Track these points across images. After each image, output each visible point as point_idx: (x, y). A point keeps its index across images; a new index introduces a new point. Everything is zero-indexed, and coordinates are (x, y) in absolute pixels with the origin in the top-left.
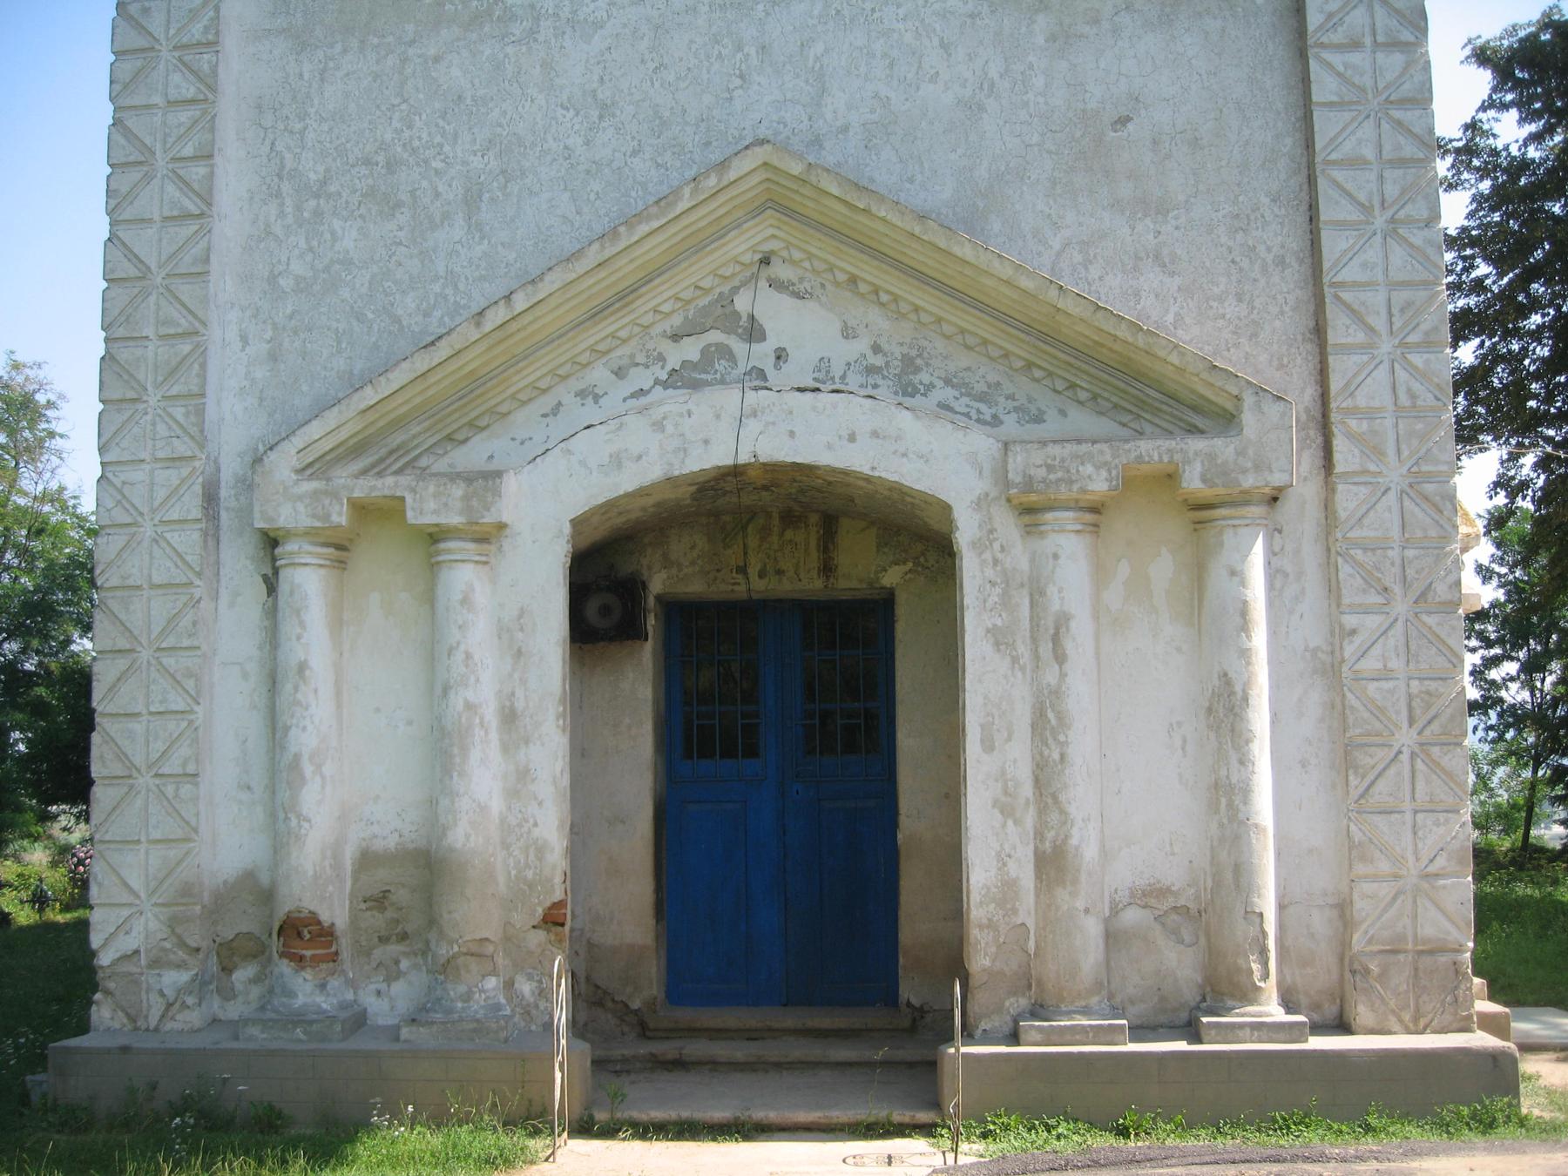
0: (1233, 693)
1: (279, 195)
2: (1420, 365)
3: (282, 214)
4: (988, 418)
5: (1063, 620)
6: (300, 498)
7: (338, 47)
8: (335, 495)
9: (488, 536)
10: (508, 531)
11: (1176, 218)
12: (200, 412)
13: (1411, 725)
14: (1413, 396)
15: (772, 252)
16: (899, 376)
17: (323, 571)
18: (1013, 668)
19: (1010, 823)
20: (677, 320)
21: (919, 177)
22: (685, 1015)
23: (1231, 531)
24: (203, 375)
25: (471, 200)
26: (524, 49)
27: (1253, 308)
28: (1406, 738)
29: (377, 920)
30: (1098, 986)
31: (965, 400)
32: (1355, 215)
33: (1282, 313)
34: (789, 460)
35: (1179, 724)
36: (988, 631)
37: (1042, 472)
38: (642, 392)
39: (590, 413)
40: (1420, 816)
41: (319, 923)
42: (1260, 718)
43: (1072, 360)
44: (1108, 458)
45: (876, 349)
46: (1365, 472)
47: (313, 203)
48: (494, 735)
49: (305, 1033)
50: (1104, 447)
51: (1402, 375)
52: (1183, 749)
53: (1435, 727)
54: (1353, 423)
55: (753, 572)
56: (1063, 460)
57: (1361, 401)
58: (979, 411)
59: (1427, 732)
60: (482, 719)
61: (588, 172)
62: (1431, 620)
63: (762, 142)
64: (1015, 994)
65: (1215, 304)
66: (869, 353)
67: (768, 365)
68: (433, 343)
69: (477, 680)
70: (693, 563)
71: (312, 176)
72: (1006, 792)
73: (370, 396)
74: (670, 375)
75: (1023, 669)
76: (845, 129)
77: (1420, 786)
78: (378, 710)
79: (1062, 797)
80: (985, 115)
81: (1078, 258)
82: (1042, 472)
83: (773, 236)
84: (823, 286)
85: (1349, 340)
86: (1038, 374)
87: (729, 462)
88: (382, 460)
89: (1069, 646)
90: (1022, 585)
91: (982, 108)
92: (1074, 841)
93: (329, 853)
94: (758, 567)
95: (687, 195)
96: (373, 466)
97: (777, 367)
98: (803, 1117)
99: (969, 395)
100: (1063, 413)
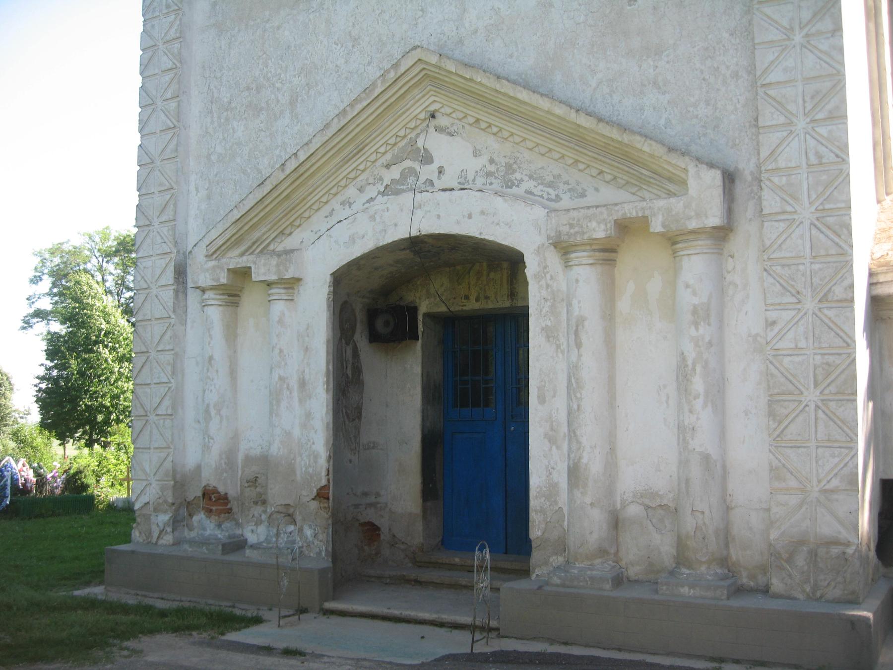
0: (686, 366)
1: (211, 112)
2: (825, 135)
3: (212, 122)
4: (553, 197)
5: (581, 321)
7: (236, 29)
9: (292, 284)
10: (302, 282)
11: (668, 56)
12: (174, 228)
13: (815, 388)
14: (819, 156)
15: (436, 111)
16: (504, 176)
17: (221, 308)
18: (557, 352)
19: (554, 447)
20: (389, 156)
21: (516, 54)
22: (444, 557)
23: (686, 258)
25: (293, 103)
26: (318, 14)
27: (716, 109)
28: (812, 396)
29: (251, 493)
31: (540, 187)
34: (437, 232)
35: (665, 386)
36: (543, 329)
39: (347, 212)
40: (820, 450)
41: (218, 493)
43: (596, 156)
44: (605, 216)
45: (492, 161)
46: (784, 212)
47: (225, 114)
48: (295, 394)
49: (207, 549)
50: (603, 209)
51: (812, 143)
52: (667, 402)
53: (832, 388)
54: (776, 180)
55: (473, 298)
56: (579, 220)
57: (782, 164)
58: (548, 194)
59: (826, 392)
60: (288, 385)
61: (347, 78)
62: (831, 313)
63: (415, 48)
64: (556, 554)
65: (691, 109)
66: (487, 164)
67: (434, 177)
68: (262, 183)
72: (552, 429)
74: (386, 188)
75: (562, 352)
76: (476, 31)
77: (821, 428)
78: (252, 381)
79: (578, 433)
80: (553, 9)
81: (606, 90)
82: (566, 229)
84: (463, 126)
85: (774, 122)
86: (581, 166)
87: (407, 236)
88: (250, 247)
89: (584, 338)
90: (563, 300)
92: (584, 461)
93: (224, 456)
94: (476, 295)
95: (379, 85)
96: (246, 251)
97: (439, 178)
99: (542, 184)
100: (597, 190)
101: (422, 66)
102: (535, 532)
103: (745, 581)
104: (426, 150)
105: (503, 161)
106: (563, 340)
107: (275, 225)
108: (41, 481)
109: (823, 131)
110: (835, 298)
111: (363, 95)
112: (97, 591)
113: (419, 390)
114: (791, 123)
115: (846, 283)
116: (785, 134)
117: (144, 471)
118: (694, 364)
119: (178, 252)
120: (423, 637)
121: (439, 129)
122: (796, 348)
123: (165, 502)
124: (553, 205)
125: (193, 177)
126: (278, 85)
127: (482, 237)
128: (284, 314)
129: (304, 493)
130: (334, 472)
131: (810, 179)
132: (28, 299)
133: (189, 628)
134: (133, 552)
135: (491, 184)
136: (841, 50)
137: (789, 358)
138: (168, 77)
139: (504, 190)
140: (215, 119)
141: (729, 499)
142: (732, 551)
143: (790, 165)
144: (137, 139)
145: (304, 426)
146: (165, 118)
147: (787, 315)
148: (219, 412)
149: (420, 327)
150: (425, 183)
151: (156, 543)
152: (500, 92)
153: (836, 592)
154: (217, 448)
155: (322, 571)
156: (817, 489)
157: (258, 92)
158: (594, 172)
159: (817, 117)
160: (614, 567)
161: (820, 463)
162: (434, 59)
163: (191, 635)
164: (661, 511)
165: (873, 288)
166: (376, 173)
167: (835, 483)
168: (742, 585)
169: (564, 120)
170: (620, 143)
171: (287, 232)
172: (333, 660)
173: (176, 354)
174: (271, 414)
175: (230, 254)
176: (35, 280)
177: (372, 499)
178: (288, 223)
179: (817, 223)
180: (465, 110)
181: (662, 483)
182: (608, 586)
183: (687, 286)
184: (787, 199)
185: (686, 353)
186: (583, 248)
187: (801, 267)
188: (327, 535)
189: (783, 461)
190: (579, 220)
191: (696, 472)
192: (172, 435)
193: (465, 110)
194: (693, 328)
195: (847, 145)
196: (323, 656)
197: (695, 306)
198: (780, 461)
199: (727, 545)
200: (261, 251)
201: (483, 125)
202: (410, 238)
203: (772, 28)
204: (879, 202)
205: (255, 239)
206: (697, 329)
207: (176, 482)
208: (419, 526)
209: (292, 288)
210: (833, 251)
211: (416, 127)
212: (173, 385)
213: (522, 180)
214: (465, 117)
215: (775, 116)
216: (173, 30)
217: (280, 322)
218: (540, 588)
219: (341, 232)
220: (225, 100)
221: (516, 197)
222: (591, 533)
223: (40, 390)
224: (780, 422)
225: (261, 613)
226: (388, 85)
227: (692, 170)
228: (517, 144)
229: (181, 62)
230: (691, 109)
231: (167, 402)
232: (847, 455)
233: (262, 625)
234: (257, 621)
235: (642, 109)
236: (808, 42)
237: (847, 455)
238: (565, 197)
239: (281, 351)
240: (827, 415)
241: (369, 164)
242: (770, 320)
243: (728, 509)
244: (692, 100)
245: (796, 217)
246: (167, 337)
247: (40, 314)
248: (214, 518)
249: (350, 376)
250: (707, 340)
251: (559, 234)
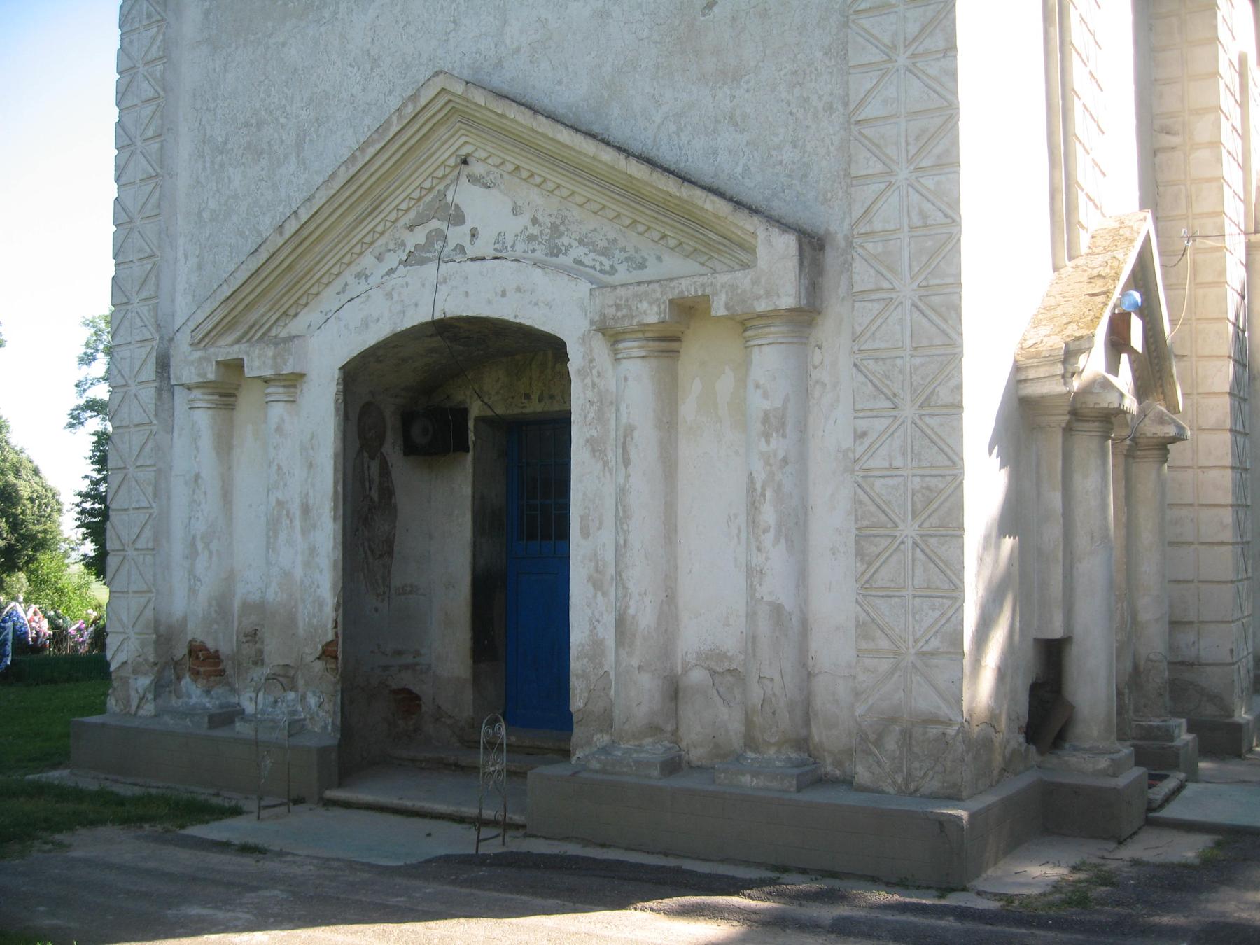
0: (755, 490)
1: (202, 156)
2: (932, 187)
3: (204, 168)
4: (607, 268)
5: (630, 429)
6: (192, 363)
8: (207, 359)
9: (294, 381)
11: (748, 82)
12: (156, 308)
13: (914, 517)
14: (922, 214)
15: (468, 155)
17: (210, 412)
19: (599, 594)
20: (412, 215)
23: (756, 349)
25: (299, 144)
27: (805, 152)
29: (248, 650)
31: (592, 255)
33: (828, 153)
35: (736, 516)
36: (587, 441)
37: (612, 311)
38: (392, 271)
39: (364, 286)
40: (917, 600)
41: (207, 650)
44: (658, 295)
45: (535, 221)
46: (879, 290)
47: (219, 158)
48: (297, 523)
50: (656, 286)
51: (915, 197)
52: (738, 536)
53: (934, 520)
55: (535, 397)
56: (627, 300)
57: (878, 225)
58: (601, 264)
59: (926, 525)
60: (288, 512)
62: (933, 422)
63: (437, 74)
64: (601, 731)
65: (774, 153)
66: (530, 225)
68: (256, 250)
69: (285, 485)
70: (497, 393)
71: (220, 139)
72: (597, 571)
75: (610, 471)
76: (518, 50)
79: (624, 576)
81: (673, 128)
82: (612, 311)
83: (466, 142)
85: (870, 172)
87: (429, 319)
88: (246, 333)
90: (612, 403)
91: (609, 15)
92: (631, 611)
93: (214, 603)
95: (395, 121)
99: (594, 251)
100: (659, 259)
101: (447, 98)
102: (577, 703)
103: (829, 769)
104: (457, 206)
105: (548, 221)
106: (611, 455)
107: (275, 304)
108: (59, 634)
109: (929, 182)
110: (940, 403)
111: (376, 136)
112: (56, 776)
113: (468, 517)
114: (891, 172)
115: (952, 383)
116: (883, 186)
117: (120, 621)
118: (763, 489)
119: (161, 338)
120: (429, 835)
121: (472, 179)
122: (891, 467)
123: (146, 660)
124: (607, 279)
125: (181, 241)
126: (283, 120)
127: (518, 321)
128: (283, 421)
129: (307, 650)
130: (344, 624)
131: (912, 246)
132: (77, 386)
133: (142, 819)
134: (103, 725)
135: (534, 251)
136: (953, 75)
137: (882, 481)
138: (148, 111)
139: (549, 259)
140: (208, 165)
141: (810, 662)
142: (814, 730)
143: (887, 228)
144: (112, 191)
145: (307, 565)
146: (145, 163)
147: (880, 425)
148: (207, 546)
149: (471, 437)
150: (455, 250)
151: (136, 714)
152: (537, 132)
153: (934, 785)
154: (205, 592)
155: (323, 752)
156: (912, 651)
157: (259, 130)
158: (656, 236)
159: (923, 164)
160: (670, 749)
161: (917, 617)
162: (459, 89)
163: (141, 827)
164: (730, 678)
165: (1021, 386)
166: (397, 236)
167: (935, 643)
168: (826, 775)
169: (613, 168)
170: (679, 198)
171: (292, 312)
172: (297, 859)
173: (159, 471)
174: (268, 549)
175: (223, 342)
176: (87, 360)
177: (409, 659)
178: (291, 302)
179: (920, 304)
180: (502, 155)
181: (730, 642)
182: (656, 773)
183: (757, 386)
184: (885, 272)
185: (755, 474)
186: (634, 336)
187: (899, 362)
188: (335, 705)
189: (872, 615)
190: (627, 300)
191: (764, 627)
192: (155, 575)
193: (502, 155)
194: (763, 440)
195: (958, 202)
196: (288, 853)
197: (766, 414)
198: (868, 614)
199: (807, 723)
200: (261, 338)
201: (525, 174)
202: (433, 322)
203: (870, 46)
204: (1056, 269)
205: (252, 322)
206: (768, 442)
207: (159, 636)
208: (468, 695)
209: (295, 387)
210: (938, 341)
211: (445, 176)
212: (155, 511)
213: (570, 246)
214: (503, 163)
215: (871, 163)
216: (155, 48)
217: (279, 429)
218: (575, 774)
219: (353, 314)
220: (220, 139)
221: (560, 269)
222: (639, 704)
223: (83, 512)
224: (869, 564)
225: (241, 803)
226: (405, 122)
227: (761, 234)
228: (565, 198)
229: (164, 89)
230: (774, 153)
231: (148, 533)
232: (950, 607)
233: (240, 817)
234: (236, 812)
235: (715, 153)
236: (914, 64)
237: (950, 607)
239: (279, 468)
240: (926, 555)
241: (388, 224)
242: (859, 431)
243: (807, 674)
244: (776, 140)
245: (894, 295)
246: (147, 449)
247: (94, 406)
248: (202, 682)
249: (376, 499)
250: (780, 457)
251: (604, 317)
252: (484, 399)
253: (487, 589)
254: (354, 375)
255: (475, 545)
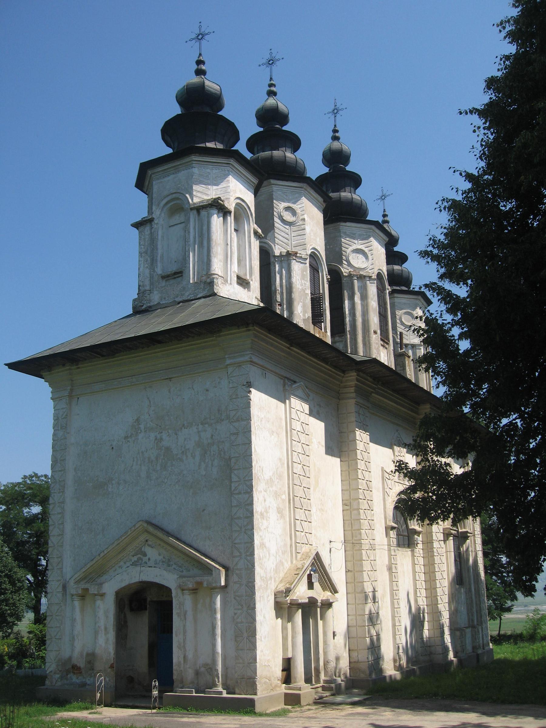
14: (248, 566)
20: (134, 552)
24: (62, 565)
30: (192, 683)
32: (239, 529)
42: (219, 631)
45: (164, 557)
48: (103, 632)
57: (238, 567)
73: (84, 570)
98: (143, 705)
102: (175, 677)
113: (147, 628)
121: (149, 545)
134: (47, 688)
138: (60, 516)
147: (239, 611)
175: (82, 583)
238: (185, 571)
252: (151, 596)
253: (152, 647)
254: (118, 594)
255: (149, 635)
